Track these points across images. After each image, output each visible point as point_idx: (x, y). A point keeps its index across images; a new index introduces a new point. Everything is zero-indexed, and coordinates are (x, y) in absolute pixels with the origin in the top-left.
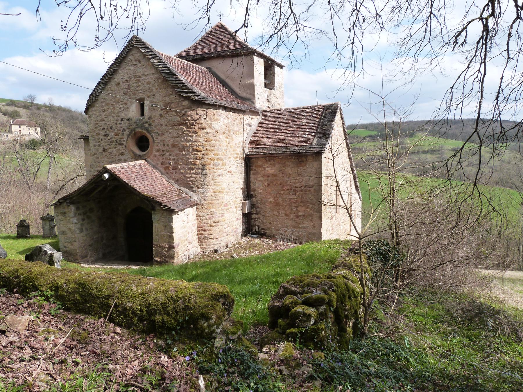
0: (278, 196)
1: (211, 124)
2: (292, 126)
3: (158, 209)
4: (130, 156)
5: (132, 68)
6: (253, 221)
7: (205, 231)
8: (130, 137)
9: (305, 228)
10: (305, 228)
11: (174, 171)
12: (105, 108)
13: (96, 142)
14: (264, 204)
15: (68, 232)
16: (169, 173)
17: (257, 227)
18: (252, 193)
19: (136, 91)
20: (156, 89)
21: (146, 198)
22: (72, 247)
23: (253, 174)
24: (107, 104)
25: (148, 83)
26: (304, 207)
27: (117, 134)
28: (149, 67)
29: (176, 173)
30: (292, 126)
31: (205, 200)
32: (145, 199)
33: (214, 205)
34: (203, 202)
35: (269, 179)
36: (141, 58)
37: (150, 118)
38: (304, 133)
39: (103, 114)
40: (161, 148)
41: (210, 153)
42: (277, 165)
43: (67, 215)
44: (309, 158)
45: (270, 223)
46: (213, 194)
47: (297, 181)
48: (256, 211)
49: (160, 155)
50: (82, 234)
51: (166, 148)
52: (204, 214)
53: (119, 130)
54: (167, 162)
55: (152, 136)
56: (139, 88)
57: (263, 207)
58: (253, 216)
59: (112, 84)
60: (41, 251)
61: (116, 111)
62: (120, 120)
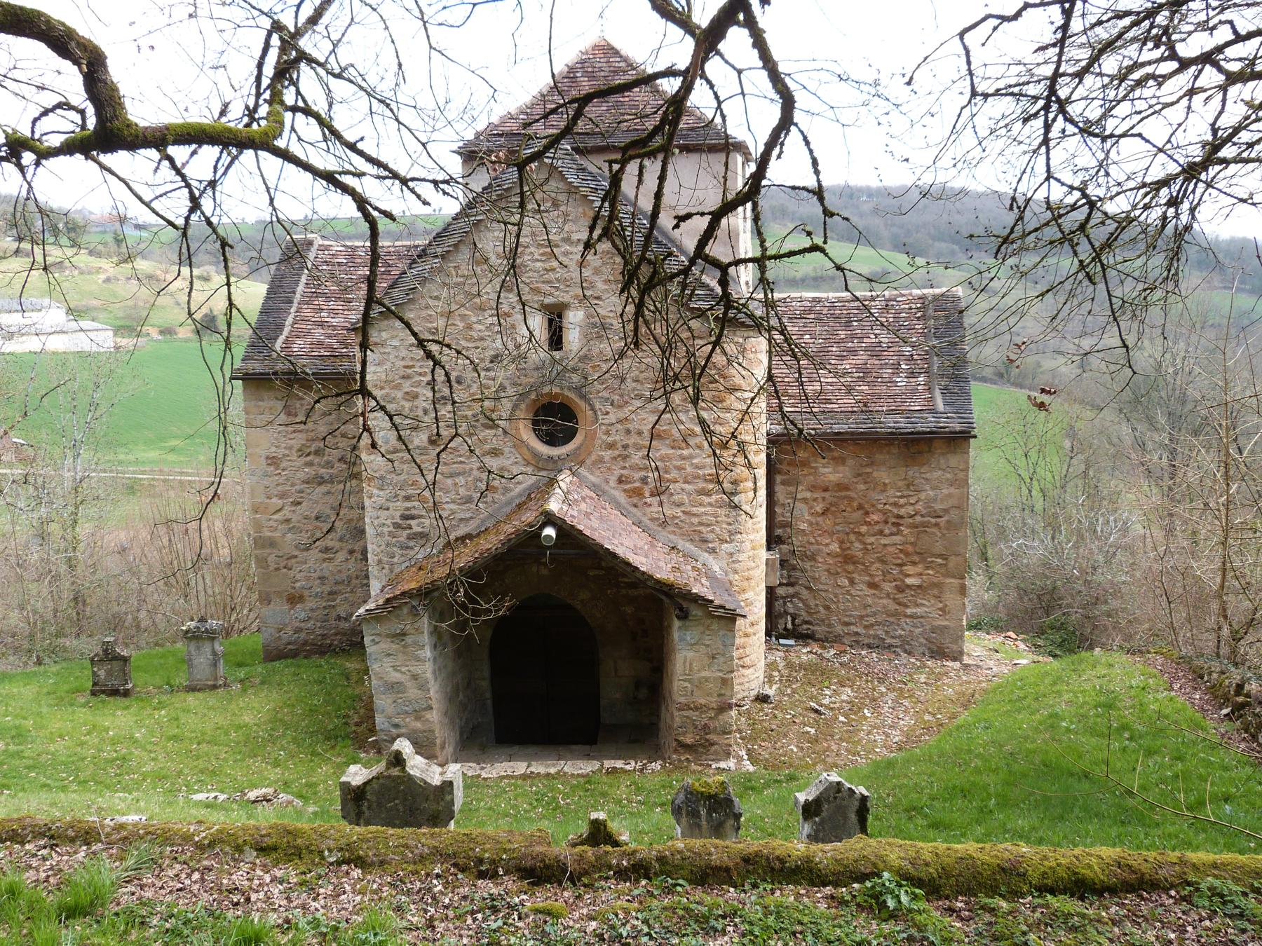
0: (852, 537)
3: (696, 616)
4: (520, 459)
8: (523, 406)
9: (922, 617)
10: (922, 617)
11: (655, 500)
14: (813, 558)
16: (640, 504)
17: (789, 618)
18: (779, 531)
19: (543, 282)
21: (665, 589)
23: (783, 483)
26: (920, 566)
30: (853, 352)
31: (736, 572)
32: (658, 590)
35: (827, 495)
40: (618, 438)
42: (851, 462)
43: (409, 640)
44: (937, 444)
45: (827, 608)
47: (902, 501)
48: (790, 576)
49: (615, 458)
55: (593, 409)
56: (551, 276)
57: (807, 565)
60: (839, 791)
62: (488, 359)
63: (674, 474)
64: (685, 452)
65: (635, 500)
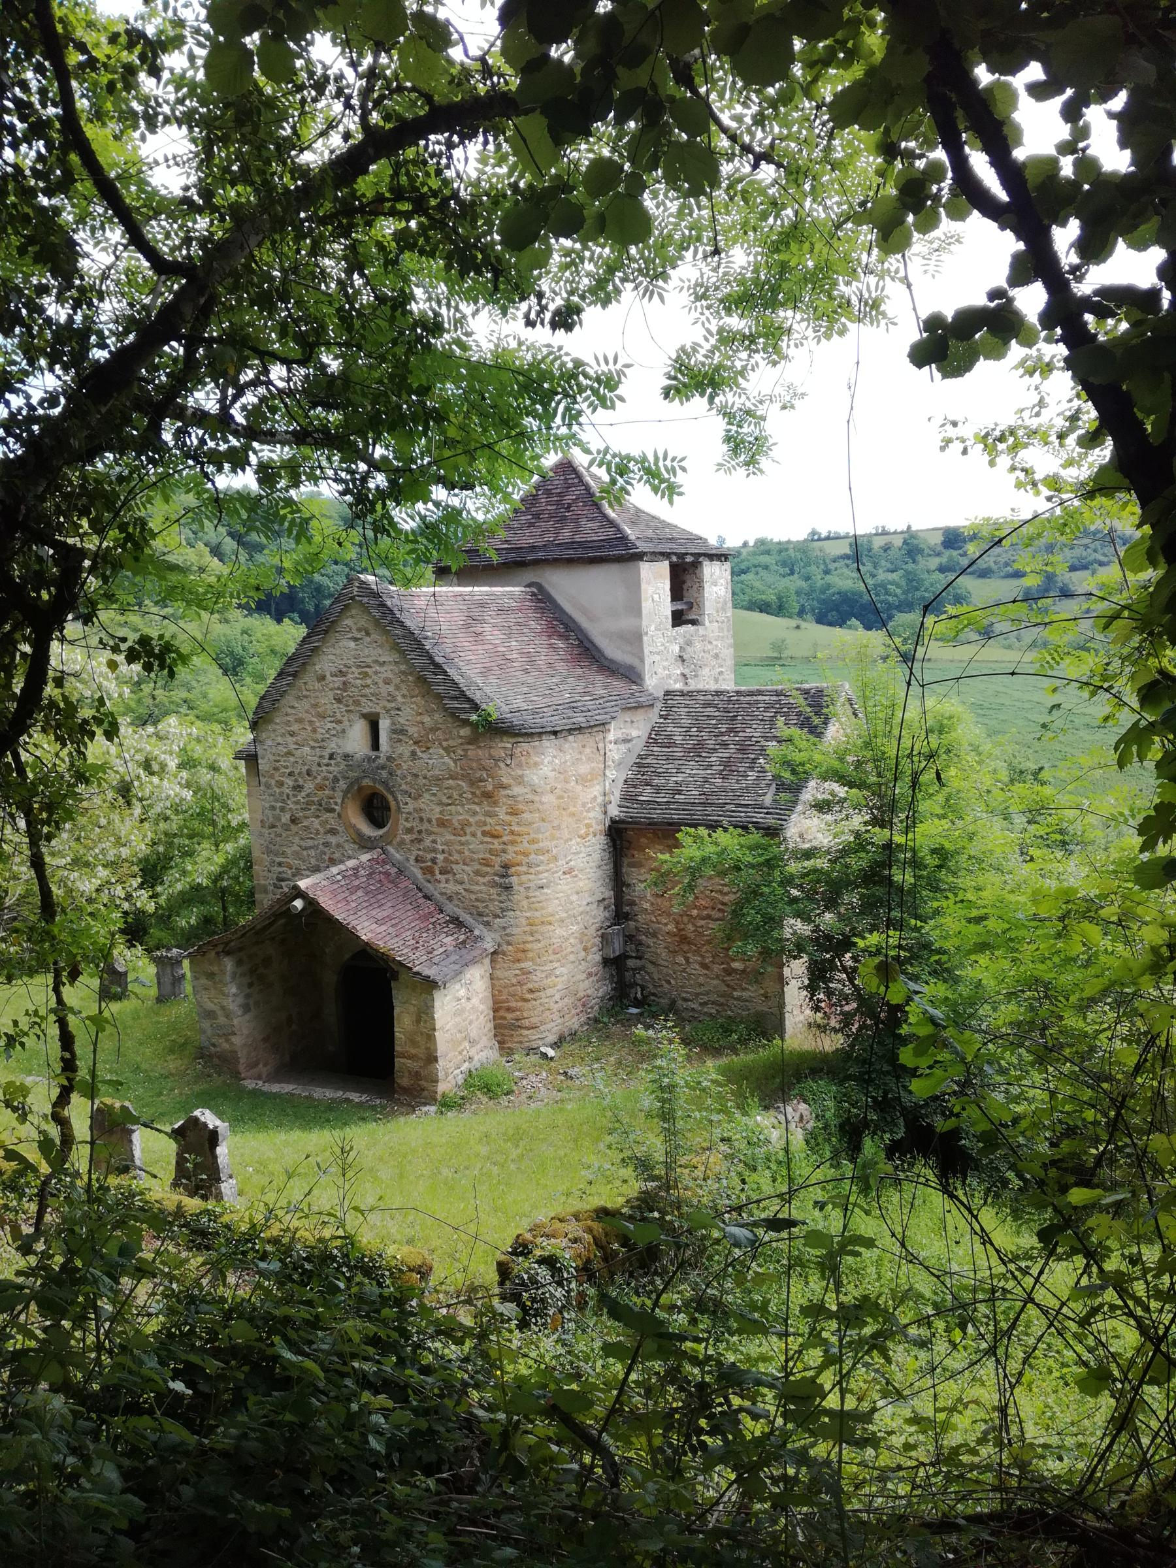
0: (685, 919)
1: (521, 776)
2: (725, 745)
5: (352, 644)
6: (628, 974)
7: (509, 1009)
12: (295, 727)
13: (276, 801)
14: (654, 935)
15: (219, 1013)
18: (627, 909)
20: (404, 696)
22: (226, 1046)
24: (300, 721)
25: (387, 682)
27: (321, 788)
28: (387, 646)
29: (447, 881)
30: (725, 745)
33: (530, 955)
34: (505, 947)
36: (371, 628)
37: (389, 758)
38: (752, 768)
39: (290, 740)
41: (519, 839)
45: (669, 982)
46: (527, 928)
47: (726, 889)
50: (247, 1017)
51: (426, 826)
52: (506, 974)
53: (325, 778)
54: (429, 856)
55: (396, 799)
56: (367, 691)
57: (650, 942)
58: (631, 963)
59: (308, 679)
61: (319, 737)
63: (456, 857)
64: (463, 839)
65: (428, 877)
